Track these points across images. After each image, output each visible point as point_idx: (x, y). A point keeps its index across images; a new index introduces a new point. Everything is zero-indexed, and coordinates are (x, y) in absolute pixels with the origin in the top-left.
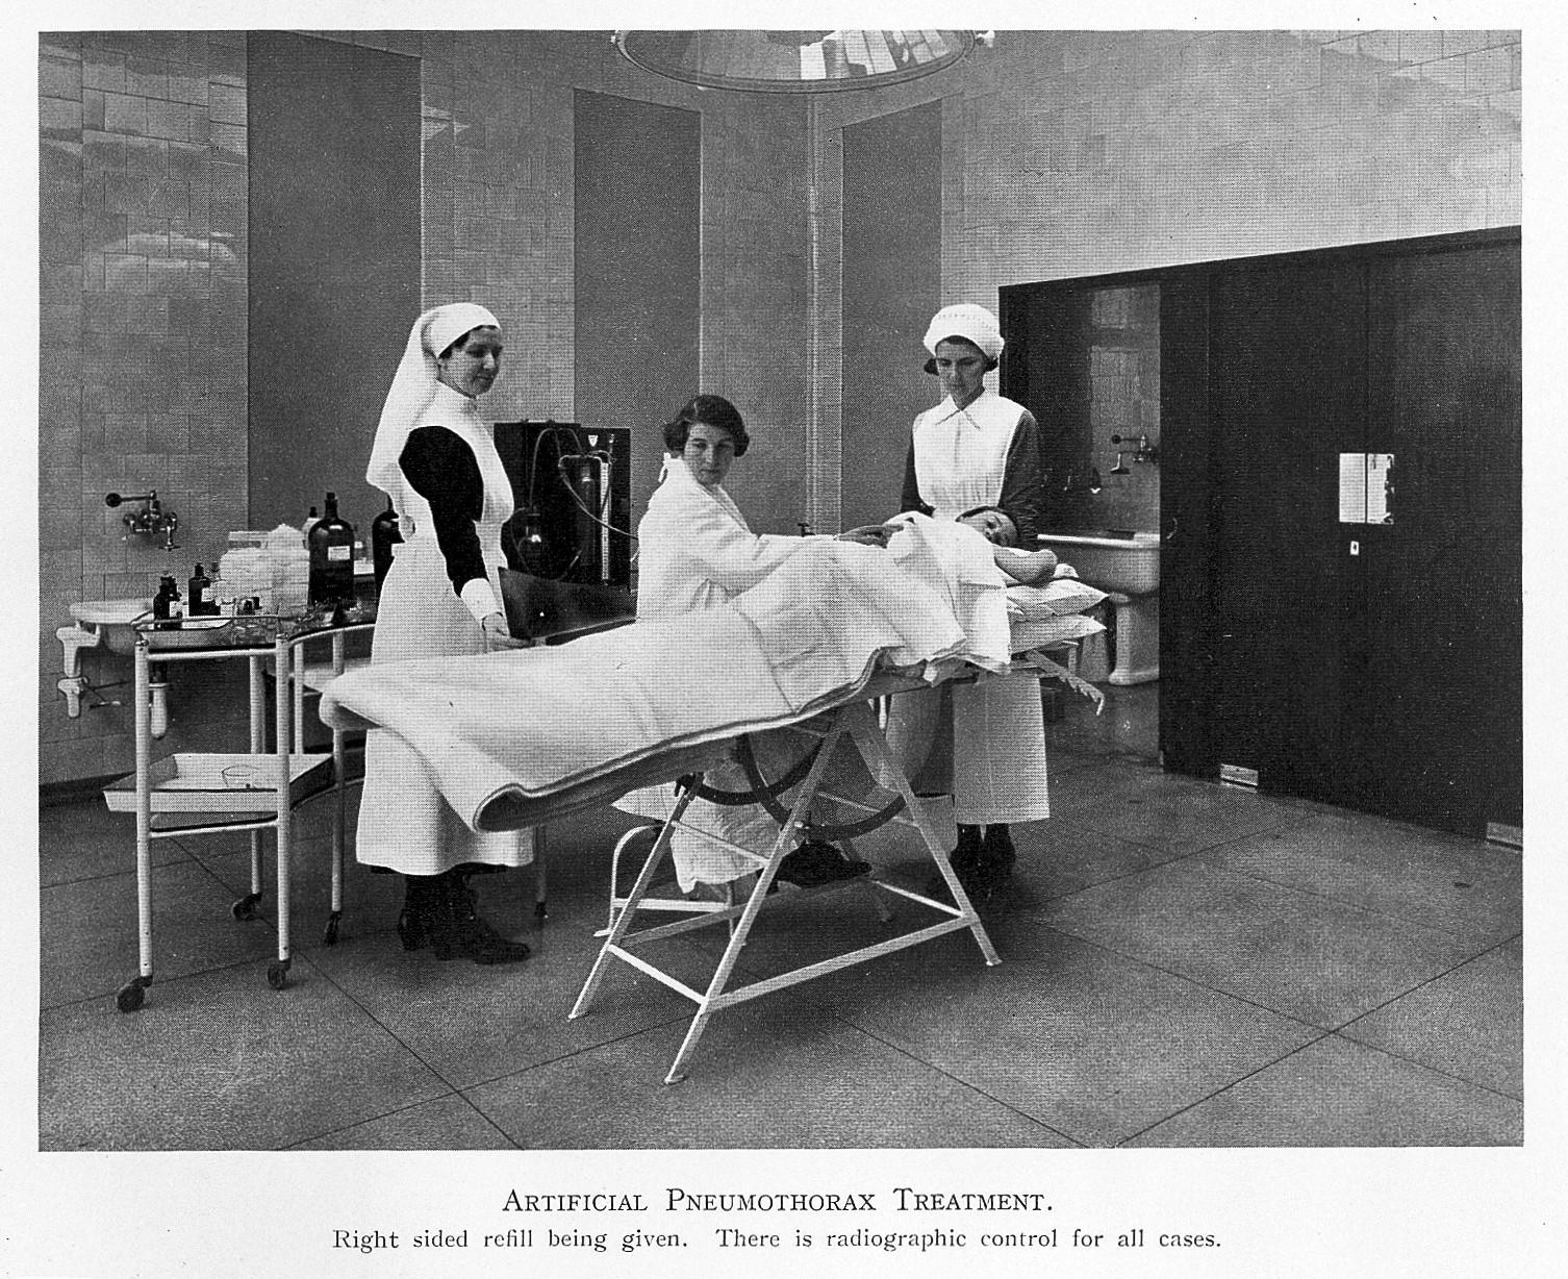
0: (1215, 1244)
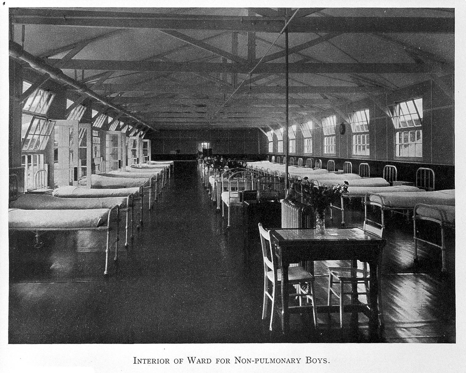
0: (328, 362)
